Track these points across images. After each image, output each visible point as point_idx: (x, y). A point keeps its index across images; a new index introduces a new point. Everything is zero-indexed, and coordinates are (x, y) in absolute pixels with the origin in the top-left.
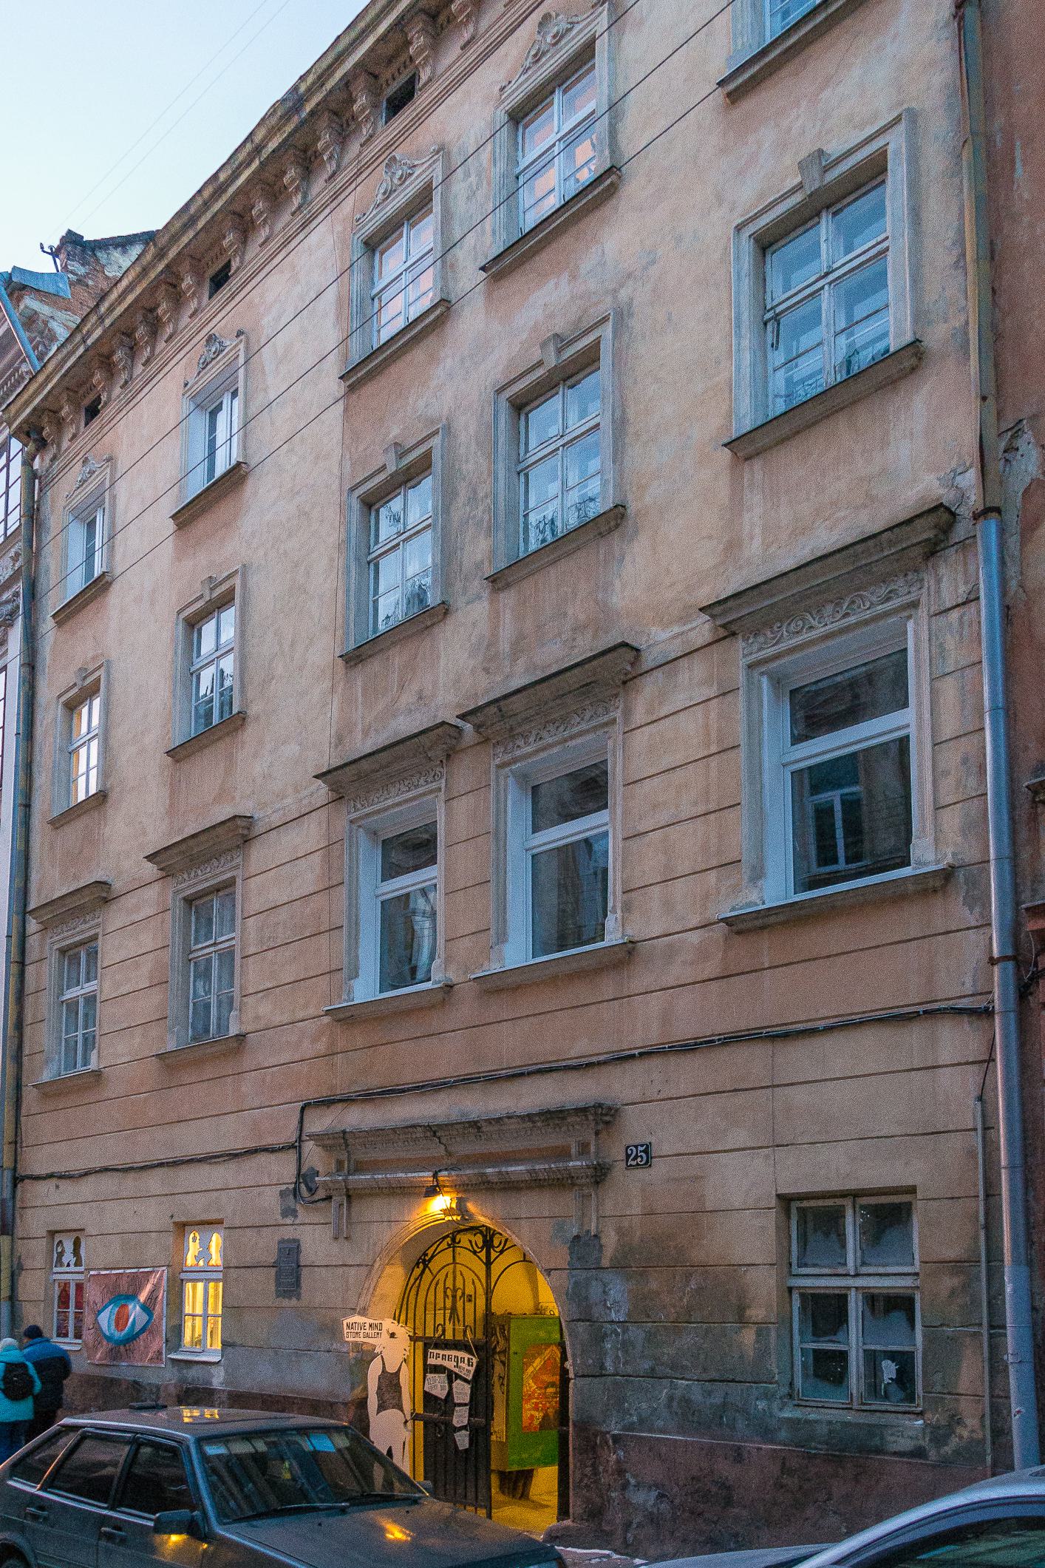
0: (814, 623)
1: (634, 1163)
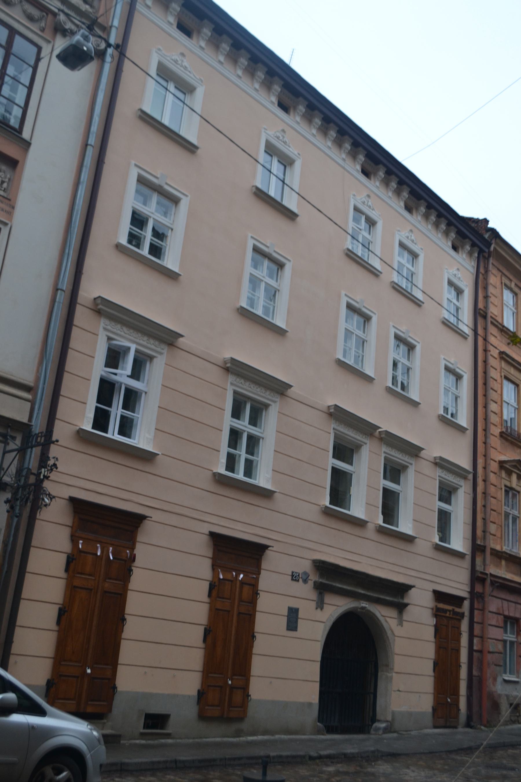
0: (252, 387)
1: (295, 579)
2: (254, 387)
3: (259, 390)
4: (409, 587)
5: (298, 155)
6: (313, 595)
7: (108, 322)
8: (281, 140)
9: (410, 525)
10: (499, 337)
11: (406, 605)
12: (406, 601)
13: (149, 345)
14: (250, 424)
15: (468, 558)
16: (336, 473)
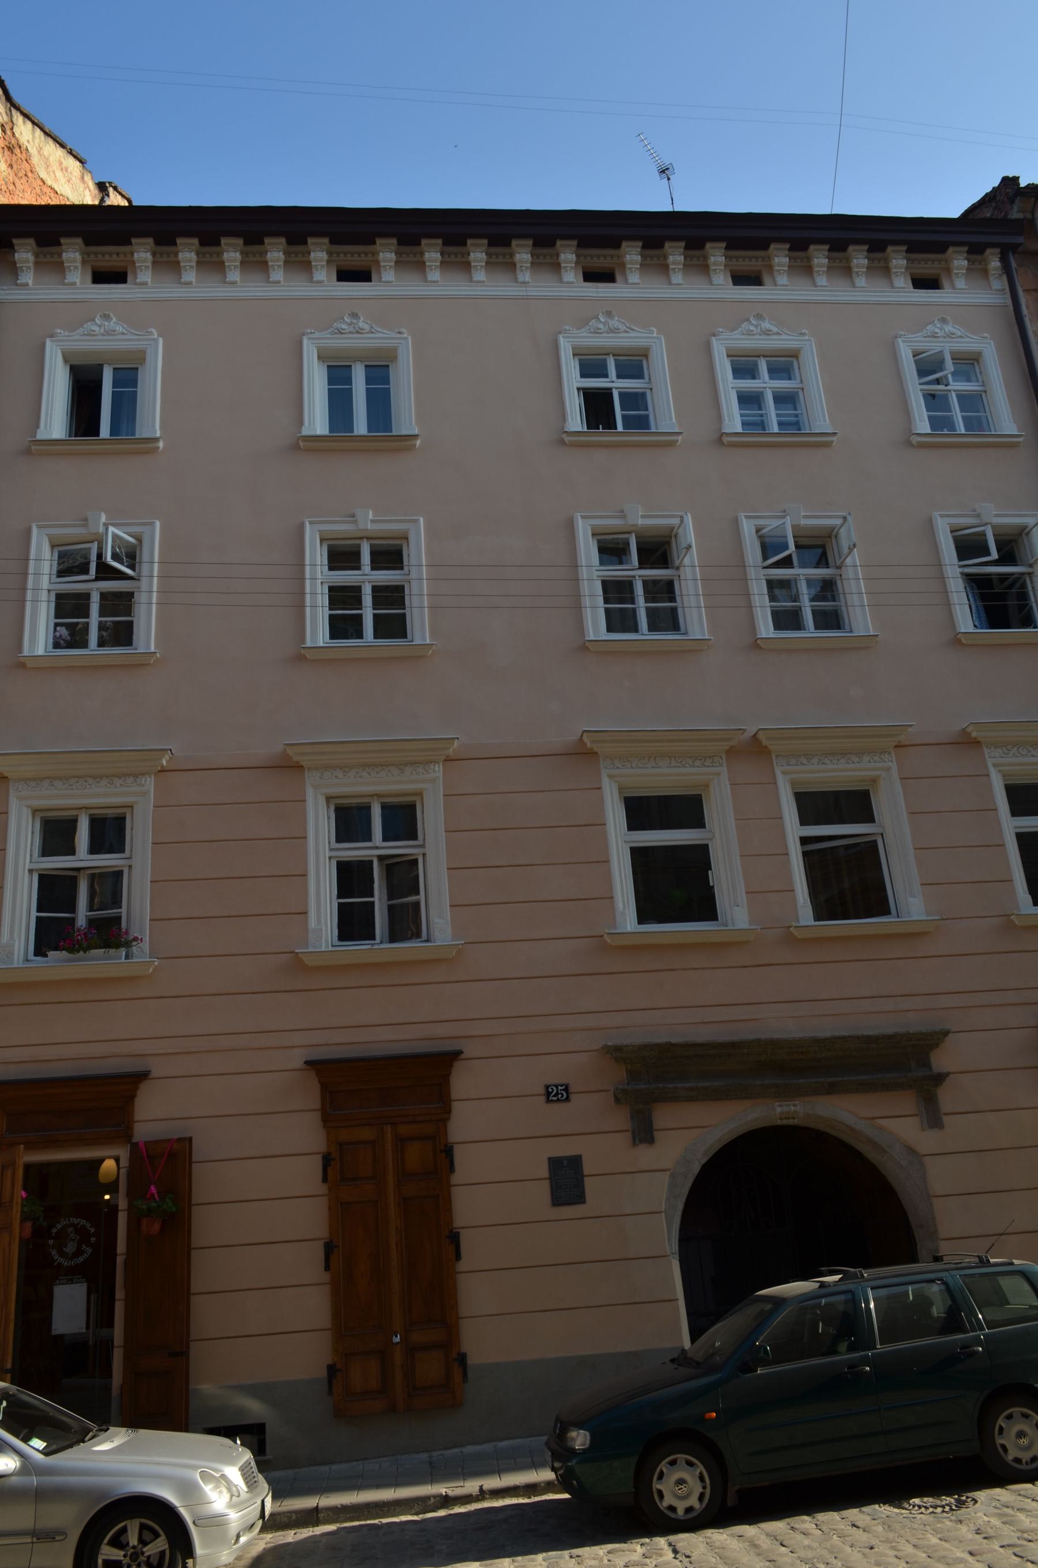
2: (369, 774)
6: (620, 1119)
8: (350, 332)
11: (940, 1078)
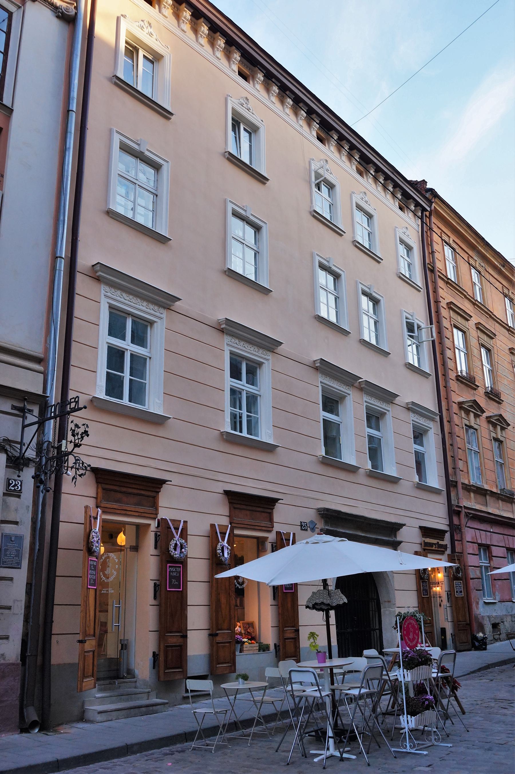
1: (13, 489)
3: (252, 349)
4: (401, 526)
5: (261, 122)
7: (107, 288)
9: (394, 468)
10: (445, 290)
11: (400, 543)
12: (399, 539)
13: (148, 310)
14: (133, 342)
15: (445, 493)
16: (326, 423)
